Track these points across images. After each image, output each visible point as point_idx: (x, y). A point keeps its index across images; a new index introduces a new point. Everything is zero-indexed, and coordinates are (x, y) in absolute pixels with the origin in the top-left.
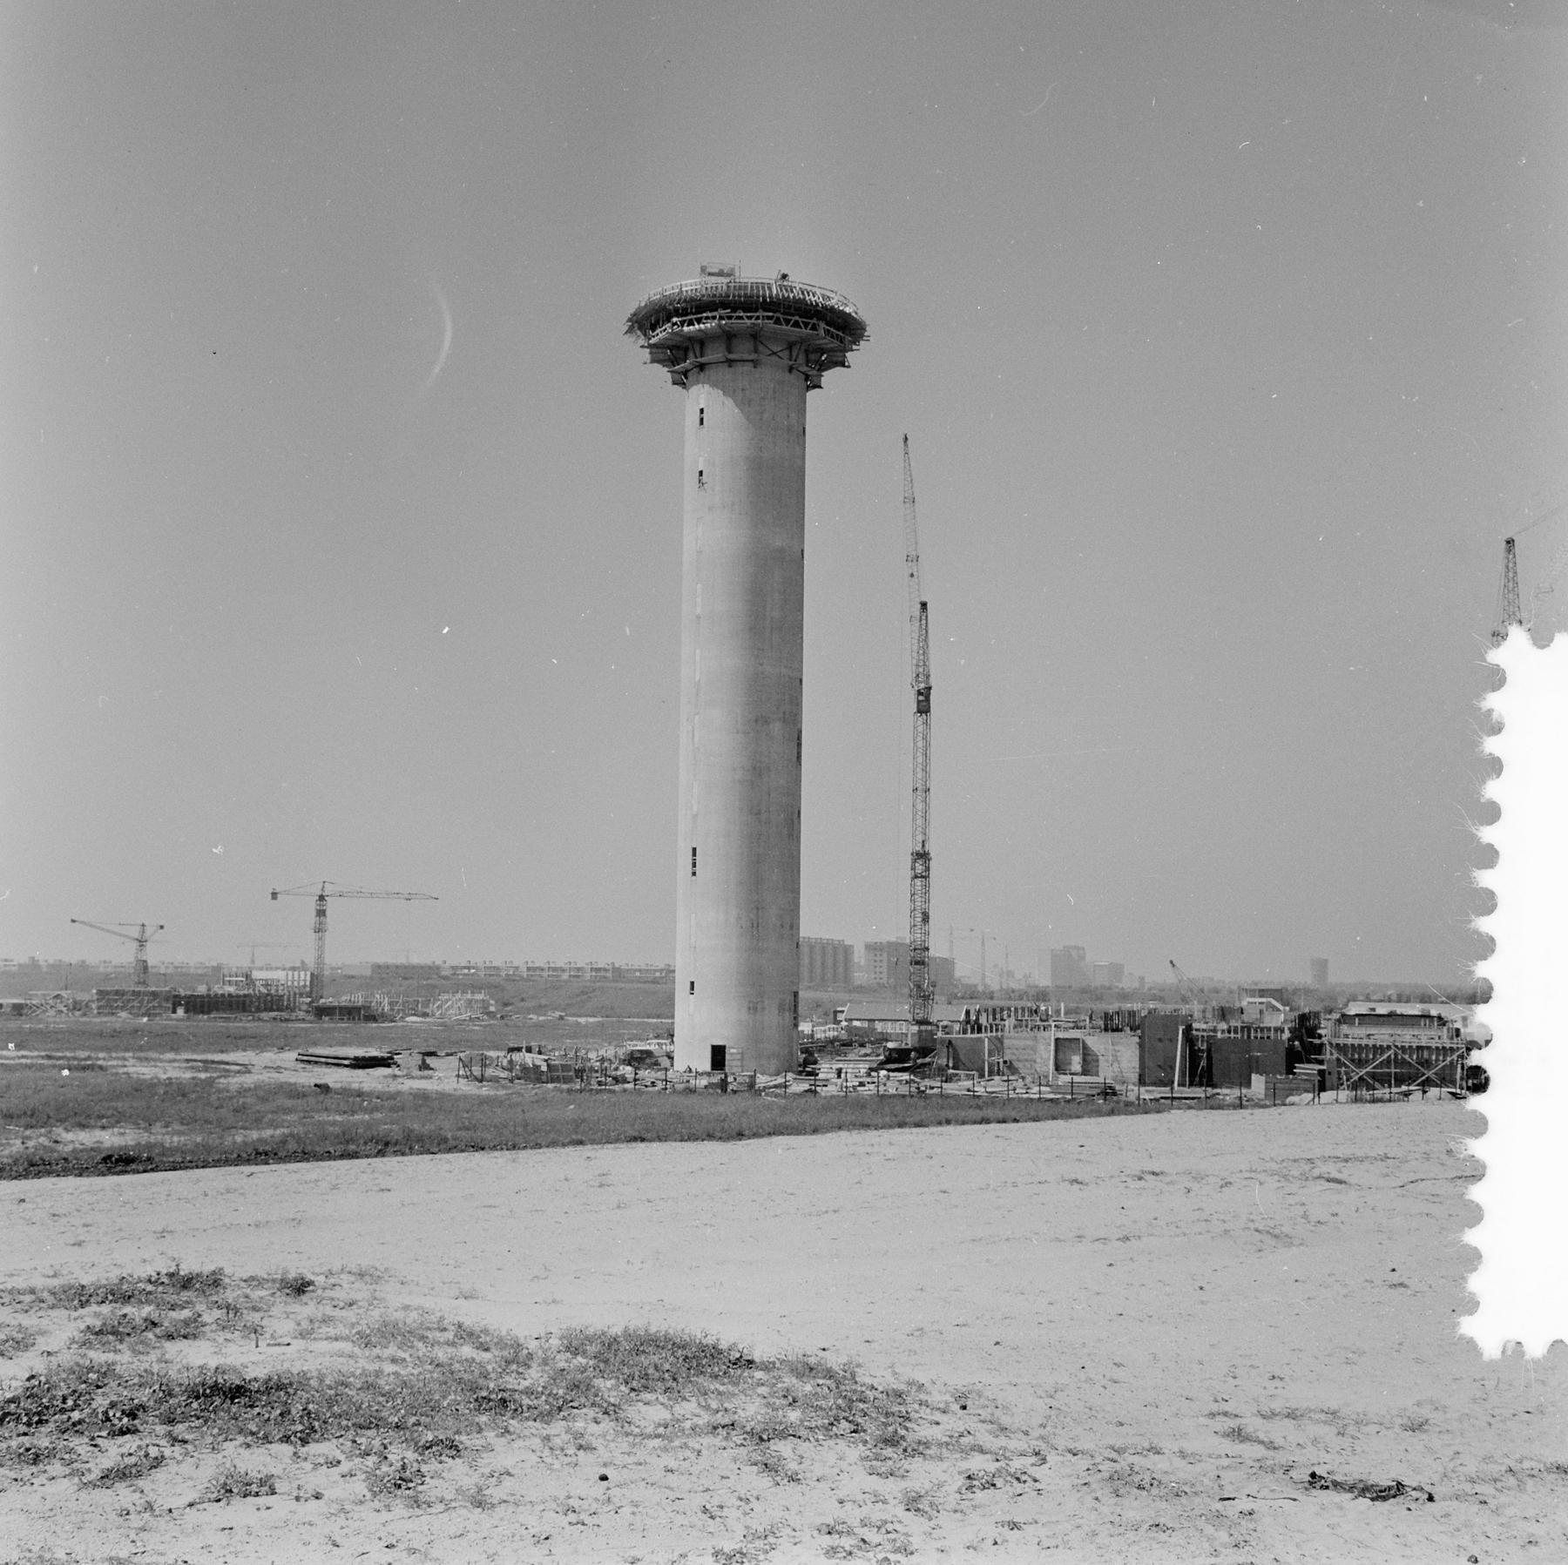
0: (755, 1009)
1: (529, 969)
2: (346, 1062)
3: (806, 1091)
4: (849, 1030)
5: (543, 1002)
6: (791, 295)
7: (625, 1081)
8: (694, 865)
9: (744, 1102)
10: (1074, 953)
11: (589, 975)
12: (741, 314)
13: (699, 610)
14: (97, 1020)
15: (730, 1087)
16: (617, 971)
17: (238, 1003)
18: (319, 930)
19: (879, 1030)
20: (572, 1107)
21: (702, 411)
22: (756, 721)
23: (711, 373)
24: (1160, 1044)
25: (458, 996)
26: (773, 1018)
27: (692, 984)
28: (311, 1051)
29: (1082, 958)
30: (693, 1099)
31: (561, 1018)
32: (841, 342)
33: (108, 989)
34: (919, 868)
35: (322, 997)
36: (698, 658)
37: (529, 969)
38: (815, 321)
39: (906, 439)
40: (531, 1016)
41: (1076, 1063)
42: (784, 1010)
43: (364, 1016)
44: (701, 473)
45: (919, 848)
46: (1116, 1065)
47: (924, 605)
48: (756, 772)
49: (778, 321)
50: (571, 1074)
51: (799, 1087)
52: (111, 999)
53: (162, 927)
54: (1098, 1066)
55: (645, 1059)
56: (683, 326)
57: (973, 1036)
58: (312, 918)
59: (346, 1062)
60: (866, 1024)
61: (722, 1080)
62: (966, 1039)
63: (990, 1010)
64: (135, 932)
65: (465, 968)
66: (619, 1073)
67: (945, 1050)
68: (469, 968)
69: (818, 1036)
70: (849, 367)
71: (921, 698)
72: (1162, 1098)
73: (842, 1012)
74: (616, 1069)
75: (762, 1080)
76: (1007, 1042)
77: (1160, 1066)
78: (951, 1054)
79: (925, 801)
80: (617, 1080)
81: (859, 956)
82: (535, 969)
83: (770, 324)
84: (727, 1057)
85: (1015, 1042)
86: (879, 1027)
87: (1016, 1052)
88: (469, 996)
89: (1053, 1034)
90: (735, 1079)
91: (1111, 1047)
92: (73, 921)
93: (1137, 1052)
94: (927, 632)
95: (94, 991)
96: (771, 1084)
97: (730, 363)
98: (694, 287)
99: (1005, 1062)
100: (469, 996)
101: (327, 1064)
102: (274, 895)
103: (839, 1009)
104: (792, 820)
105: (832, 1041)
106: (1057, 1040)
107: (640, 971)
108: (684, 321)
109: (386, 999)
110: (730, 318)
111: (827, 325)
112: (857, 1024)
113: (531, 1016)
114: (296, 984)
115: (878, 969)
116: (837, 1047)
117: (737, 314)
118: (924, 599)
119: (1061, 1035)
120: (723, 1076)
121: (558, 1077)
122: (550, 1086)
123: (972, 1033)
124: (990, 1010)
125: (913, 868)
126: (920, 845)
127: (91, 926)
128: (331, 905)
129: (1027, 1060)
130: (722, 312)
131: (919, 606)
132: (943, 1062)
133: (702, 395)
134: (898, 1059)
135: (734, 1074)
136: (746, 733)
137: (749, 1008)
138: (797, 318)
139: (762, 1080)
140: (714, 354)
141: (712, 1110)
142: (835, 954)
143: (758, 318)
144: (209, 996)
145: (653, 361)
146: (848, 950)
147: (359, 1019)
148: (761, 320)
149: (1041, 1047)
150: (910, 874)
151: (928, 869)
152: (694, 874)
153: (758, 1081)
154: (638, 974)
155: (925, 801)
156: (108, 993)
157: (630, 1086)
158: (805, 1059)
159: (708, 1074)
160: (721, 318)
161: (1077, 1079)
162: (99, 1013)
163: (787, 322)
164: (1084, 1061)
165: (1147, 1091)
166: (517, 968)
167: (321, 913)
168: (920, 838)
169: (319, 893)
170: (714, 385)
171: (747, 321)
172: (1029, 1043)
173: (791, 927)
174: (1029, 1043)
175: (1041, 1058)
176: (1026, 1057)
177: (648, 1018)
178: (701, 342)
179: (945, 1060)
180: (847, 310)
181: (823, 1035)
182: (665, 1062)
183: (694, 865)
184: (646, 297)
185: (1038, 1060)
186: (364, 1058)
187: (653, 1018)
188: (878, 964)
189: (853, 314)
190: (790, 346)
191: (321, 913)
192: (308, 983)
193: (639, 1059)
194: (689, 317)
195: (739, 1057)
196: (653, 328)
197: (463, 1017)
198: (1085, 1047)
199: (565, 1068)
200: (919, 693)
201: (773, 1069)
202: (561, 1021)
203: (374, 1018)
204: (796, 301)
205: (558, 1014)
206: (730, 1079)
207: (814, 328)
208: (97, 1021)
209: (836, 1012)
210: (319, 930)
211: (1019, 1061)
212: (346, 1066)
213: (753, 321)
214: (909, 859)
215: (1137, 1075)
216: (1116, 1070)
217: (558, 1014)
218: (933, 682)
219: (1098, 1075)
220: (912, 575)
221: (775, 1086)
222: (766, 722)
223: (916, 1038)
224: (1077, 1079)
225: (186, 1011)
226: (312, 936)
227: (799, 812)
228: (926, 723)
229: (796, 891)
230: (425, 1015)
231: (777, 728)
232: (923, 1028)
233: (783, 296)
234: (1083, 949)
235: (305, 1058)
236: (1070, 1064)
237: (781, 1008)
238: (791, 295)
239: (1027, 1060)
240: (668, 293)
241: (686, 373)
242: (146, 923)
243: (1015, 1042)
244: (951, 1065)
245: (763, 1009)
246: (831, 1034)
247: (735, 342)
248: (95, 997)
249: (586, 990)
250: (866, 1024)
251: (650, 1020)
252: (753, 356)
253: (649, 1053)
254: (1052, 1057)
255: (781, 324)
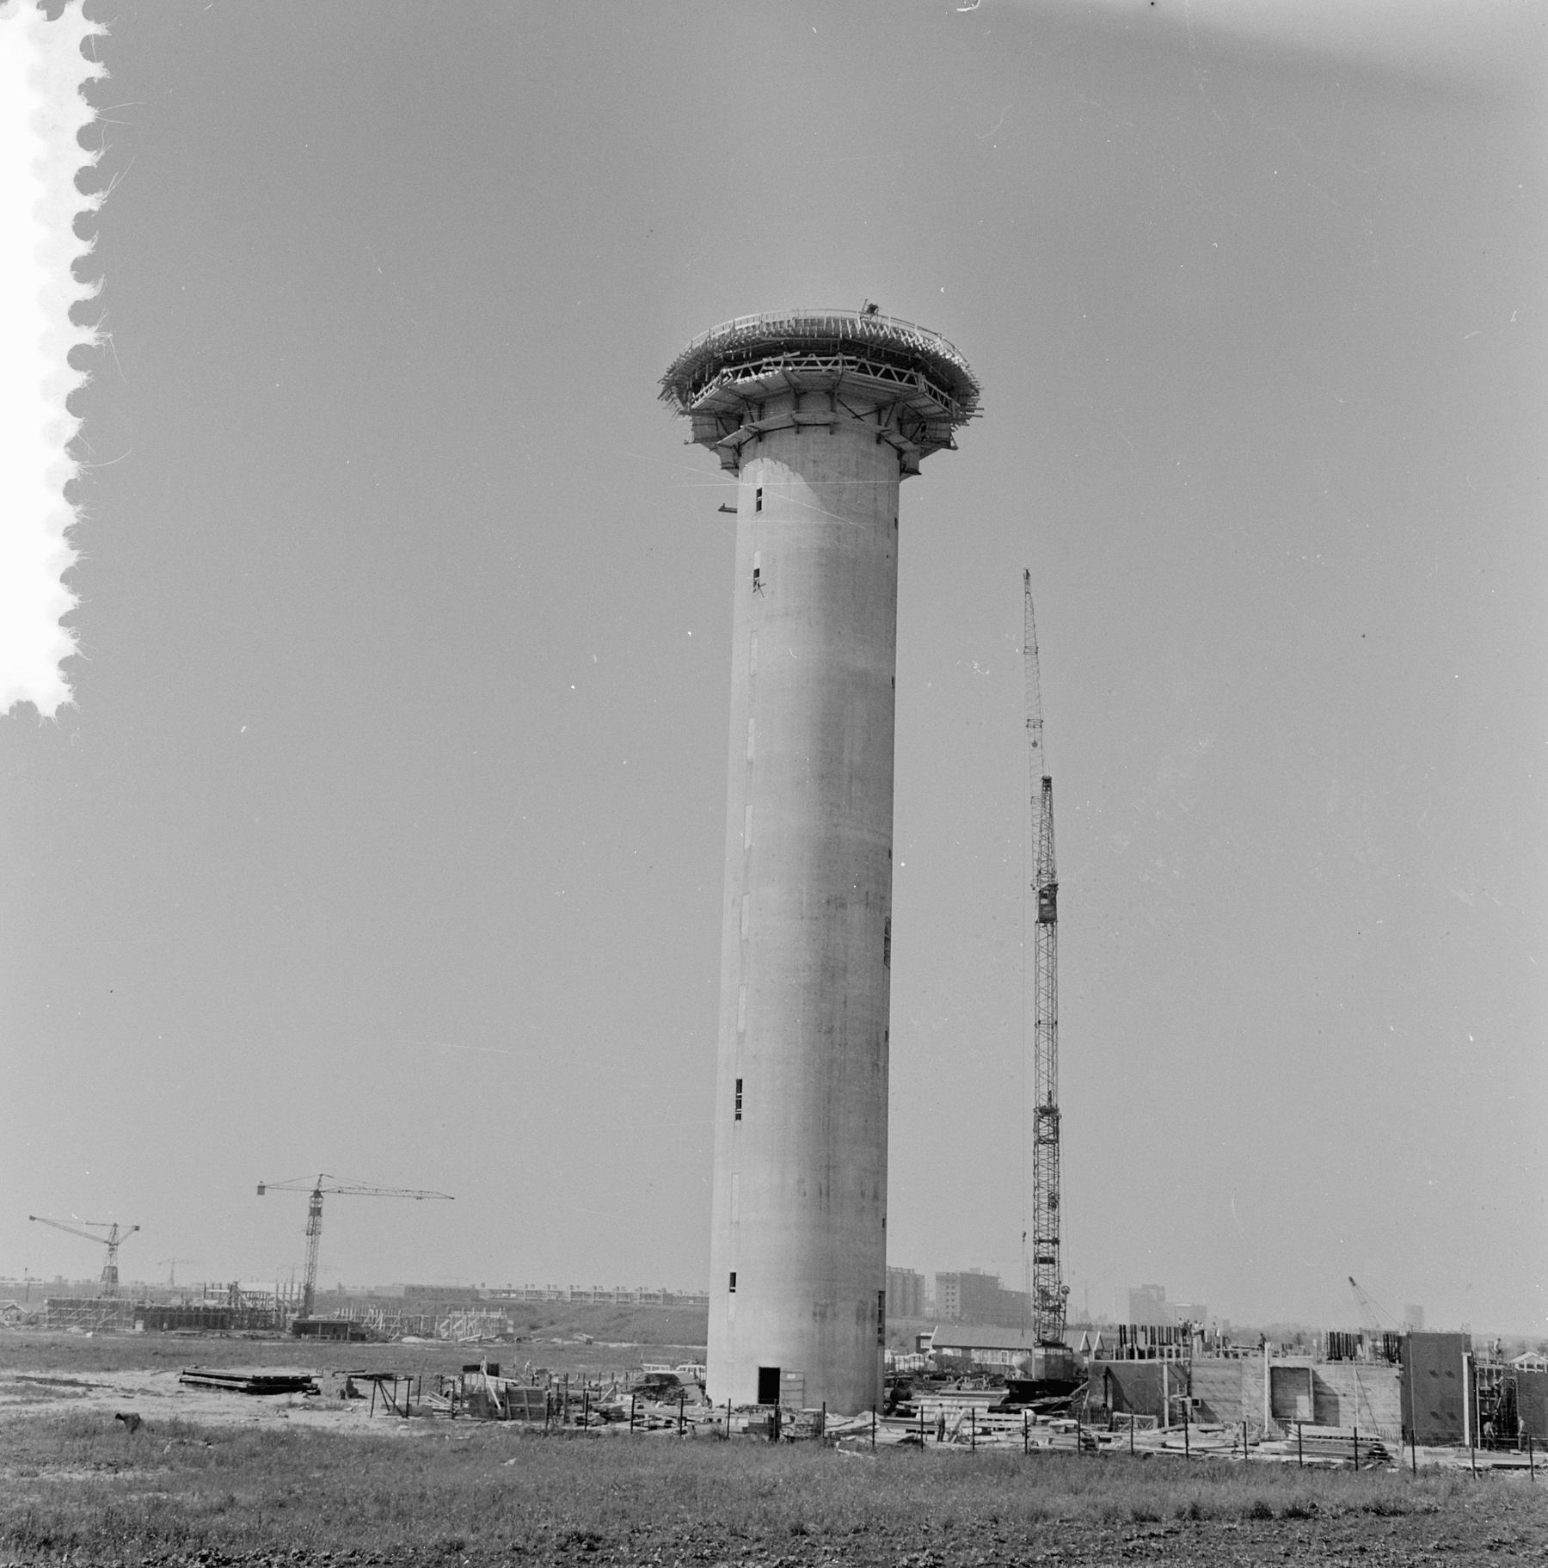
0: (823, 1315)
1: (573, 1294)
2: (242, 1385)
3: (905, 1441)
4: (940, 1360)
5: (576, 1325)
6: (881, 333)
7: (620, 1417)
8: (739, 1104)
9: (806, 1458)
10: (1153, 1292)
11: (637, 1302)
12: (814, 359)
13: (750, 754)
14: (48, 1334)
15: (785, 1432)
16: (669, 1298)
17: (216, 1318)
18: (313, 1232)
19: (976, 1361)
20: (512, 1462)
21: (760, 492)
22: (828, 902)
23: (772, 442)
24: (1433, 1379)
25: (471, 1314)
26: (850, 1330)
27: (733, 1276)
28: (205, 1370)
29: (1162, 1299)
30: (724, 1450)
31: (589, 1342)
32: (947, 405)
33: (63, 1298)
34: (1045, 1130)
35: (311, 1313)
36: (748, 816)
37: (573, 1294)
38: (912, 372)
39: (1028, 574)
40: (555, 1340)
41: (1304, 1407)
42: (864, 1319)
43: (351, 1334)
44: (757, 573)
45: (1044, 1103)
46: (1365, 1410)
47: (1047, 782)
48: (829, 971)
49: (863, 369)
50: (542, 1405)
51: (891, 1434)
52: (65, 1307)
53: (137, 1228)
54: (1338, 1412)
55: (666, 1387)
56: (735, 377)
57: (1143, 1362)
58: (304, 1218)
59: (242, 1385)
60: (959, 1353)
61: (770, 1418)
62: (1133, 1365)
63: (1149, 1329)
64: (106, 1234)
65: (504, 1291)
66: (611, 1406)
67: (1102, 1382)
68: (509, 1292)
69: (901, 1366)
70: (955, 448)
71: (1044, 901)
72: (1496, 1466)
73: (929, 1338)
74: (609, 1400)
75: (833, 1422)
76: (1196, 1373)
77: (1434, 1414)
78: (1110, 1388)
79: (1052, 1039)
80: (607, 1416)
81: (931, 1291)
82: (580, 1294)
83: (853, 373)
84: (782, 1386)
85: (1210, 1372)
86: (976, 1356)
87: (1211, 1387)
88: (484, 1314)
89: (1265, 1362)
90: (793, 1419)
91: (1357, 1383)
92: (32, 1218)
93: (1398, 1391)
94: (1051, 816)
95: (46, 1301)
96: (848, 1427)
97: (799, 426)
98: (750, 324)
99: (1195, 1402)
100: (484, 1314)
101: (219, 1387)
102: (261, 1189)
103: (923, 1334)
104: (878, 1044)
105: (920, 1373)
106: (1273, 1370)
107: (694, 1298)
108: (737, 372)
109: (382, 1315)
110: (798, 364)
111: (927, 379)
112: (947, 1352)
113: (555, 1340)
114: (287, 1297)
115: (949, 1303)
116: (937, 1378)
117: (809, 359)
118: (1047, 774)
119: (1278, 1362)
120: (773, 1413)
121: (522, 1410)
122: (507, 1424)
123: (1117, 1359)
124: (1149, 1329)
125: (1037, 1130)
126: (1046, 1098)
127: (54, 1225)
128: (327, 1203)
129: (1227, 1400)
130: (788, 356)
131: (1041, 784)
132: (1098, 1400)
133: (760, 471)
134: (1022, 1392)
135: (790, 1410)
136: (815, 919)
137: (815, 1314)
138: (888, 366)
139: (833, 1422)
140: (777, 416)
141: (750, 1472)
142: (904, 1284)
143: (836, 363)
144: (189, 1308)
145: (696, 441)
146: (918, 1281)
147: (345, 1338)
148: (841, 367)
149: (1249, 1380)
150: (1032, 1137)
151: (1056, 1131)
152: (739, 1117)
153: (827, 1423)
154: (691, 1302)
155: (1052, 1039)
156: (61, 1303)
157: (624, 1426)
158: (892, 1394)
159: (750, 1409)
160: (787, 364)
161: (1306, 1430)
162: (50, 1327)
163: (876, 371)
164: (1317, 1405)
165: (1426, 1453)
166: (560, 1293)
167: (316, 1212)
168: (1044, 1089)
169: (315, 1188)
170: (776, 458)
171: (820, 367)
172: (1232, 1373)
173: (876, 1197)
174: (1232, 1373)
175: (1250, 1398)
176: (1226, 1395)
177: (694, 1344)
178: (757, 402)
179: (1102, 1397)
180: (957, 360)
181: (907, 1366)
182: (693, 1392)
183: (739, 1104)
184: (687, 346)
185: (1245, 1401)
186: (267, 1379)
187: (698, 1345)
188: (949, 1297)
189: (963, 368)
190: (879, 410)
191: (316, 1212)
192: (302, 1297)
193: (663, 1387)
194: (744, 366)
195: (800, 1386)
196: (697, 388)
197: (471, 1339)
198: (1317, 1383)
199: (535, 1396)
200: (1042, 895)
201: (848, 1407)
202: (588, 1346)
203: (363, 1338)
204: (888, 342)
205: (586, 1336)
206: (785, 1419)
207: (911, 380)
208: (45, 1335)
209: (919, 1338)
210: (313, 1232)
211: (1215, 1400)
212: (242, 1390)
213: (829, 367)
214: (1031, 1117)
215: (1399, 1427)
216: (1366, 1418)
217: (586, 1336)
218: (1059, 879)
219: (1336, 1424)
220: (1035, 744)
221: (854, 1432)
222: (843, 906)
223: (1042, 1366)
224: (1306, 1430)
225: (145, 1327)
226: (305, 1239)
227: (887, 1033)
228: (1052, 935)
229: (882, 1146)
230: (429, 1335)
231: (856, 915)
232: (1052, 1351)
233: (871, 335)
234: (1163, 1289)
235: (192, 1378)
236: (1295, 1407)
237: (860, 1315)
238: (881, 333)
239: (1227, 1400)
240: (716, 336)
241: (738, 449)
242: (117, 1223)
243: (1210, 1372)
244: (1110, 1405)
245: (835, 1315)
246: (917, 1365)
247: (805, 402)
248: (47, 1309)
249: (623, 1312)
250: (959, 1353)
251: (695, 1347)
252: (829, 418)
253: (672, 1380)
254: (1267, 1397)
255: (868, 373)
